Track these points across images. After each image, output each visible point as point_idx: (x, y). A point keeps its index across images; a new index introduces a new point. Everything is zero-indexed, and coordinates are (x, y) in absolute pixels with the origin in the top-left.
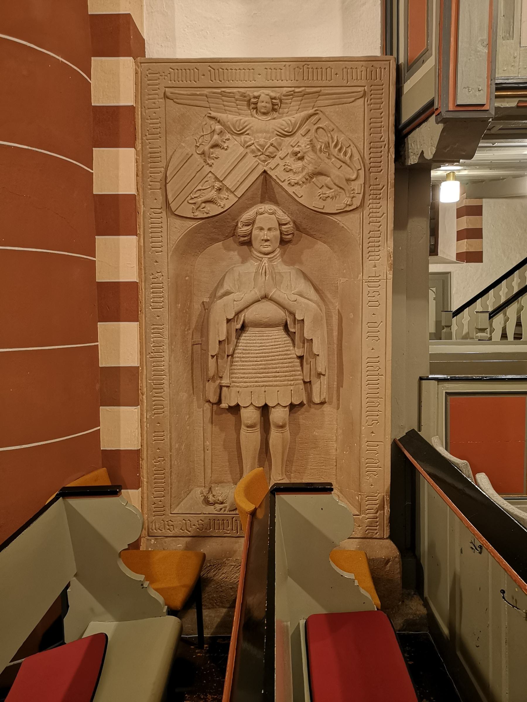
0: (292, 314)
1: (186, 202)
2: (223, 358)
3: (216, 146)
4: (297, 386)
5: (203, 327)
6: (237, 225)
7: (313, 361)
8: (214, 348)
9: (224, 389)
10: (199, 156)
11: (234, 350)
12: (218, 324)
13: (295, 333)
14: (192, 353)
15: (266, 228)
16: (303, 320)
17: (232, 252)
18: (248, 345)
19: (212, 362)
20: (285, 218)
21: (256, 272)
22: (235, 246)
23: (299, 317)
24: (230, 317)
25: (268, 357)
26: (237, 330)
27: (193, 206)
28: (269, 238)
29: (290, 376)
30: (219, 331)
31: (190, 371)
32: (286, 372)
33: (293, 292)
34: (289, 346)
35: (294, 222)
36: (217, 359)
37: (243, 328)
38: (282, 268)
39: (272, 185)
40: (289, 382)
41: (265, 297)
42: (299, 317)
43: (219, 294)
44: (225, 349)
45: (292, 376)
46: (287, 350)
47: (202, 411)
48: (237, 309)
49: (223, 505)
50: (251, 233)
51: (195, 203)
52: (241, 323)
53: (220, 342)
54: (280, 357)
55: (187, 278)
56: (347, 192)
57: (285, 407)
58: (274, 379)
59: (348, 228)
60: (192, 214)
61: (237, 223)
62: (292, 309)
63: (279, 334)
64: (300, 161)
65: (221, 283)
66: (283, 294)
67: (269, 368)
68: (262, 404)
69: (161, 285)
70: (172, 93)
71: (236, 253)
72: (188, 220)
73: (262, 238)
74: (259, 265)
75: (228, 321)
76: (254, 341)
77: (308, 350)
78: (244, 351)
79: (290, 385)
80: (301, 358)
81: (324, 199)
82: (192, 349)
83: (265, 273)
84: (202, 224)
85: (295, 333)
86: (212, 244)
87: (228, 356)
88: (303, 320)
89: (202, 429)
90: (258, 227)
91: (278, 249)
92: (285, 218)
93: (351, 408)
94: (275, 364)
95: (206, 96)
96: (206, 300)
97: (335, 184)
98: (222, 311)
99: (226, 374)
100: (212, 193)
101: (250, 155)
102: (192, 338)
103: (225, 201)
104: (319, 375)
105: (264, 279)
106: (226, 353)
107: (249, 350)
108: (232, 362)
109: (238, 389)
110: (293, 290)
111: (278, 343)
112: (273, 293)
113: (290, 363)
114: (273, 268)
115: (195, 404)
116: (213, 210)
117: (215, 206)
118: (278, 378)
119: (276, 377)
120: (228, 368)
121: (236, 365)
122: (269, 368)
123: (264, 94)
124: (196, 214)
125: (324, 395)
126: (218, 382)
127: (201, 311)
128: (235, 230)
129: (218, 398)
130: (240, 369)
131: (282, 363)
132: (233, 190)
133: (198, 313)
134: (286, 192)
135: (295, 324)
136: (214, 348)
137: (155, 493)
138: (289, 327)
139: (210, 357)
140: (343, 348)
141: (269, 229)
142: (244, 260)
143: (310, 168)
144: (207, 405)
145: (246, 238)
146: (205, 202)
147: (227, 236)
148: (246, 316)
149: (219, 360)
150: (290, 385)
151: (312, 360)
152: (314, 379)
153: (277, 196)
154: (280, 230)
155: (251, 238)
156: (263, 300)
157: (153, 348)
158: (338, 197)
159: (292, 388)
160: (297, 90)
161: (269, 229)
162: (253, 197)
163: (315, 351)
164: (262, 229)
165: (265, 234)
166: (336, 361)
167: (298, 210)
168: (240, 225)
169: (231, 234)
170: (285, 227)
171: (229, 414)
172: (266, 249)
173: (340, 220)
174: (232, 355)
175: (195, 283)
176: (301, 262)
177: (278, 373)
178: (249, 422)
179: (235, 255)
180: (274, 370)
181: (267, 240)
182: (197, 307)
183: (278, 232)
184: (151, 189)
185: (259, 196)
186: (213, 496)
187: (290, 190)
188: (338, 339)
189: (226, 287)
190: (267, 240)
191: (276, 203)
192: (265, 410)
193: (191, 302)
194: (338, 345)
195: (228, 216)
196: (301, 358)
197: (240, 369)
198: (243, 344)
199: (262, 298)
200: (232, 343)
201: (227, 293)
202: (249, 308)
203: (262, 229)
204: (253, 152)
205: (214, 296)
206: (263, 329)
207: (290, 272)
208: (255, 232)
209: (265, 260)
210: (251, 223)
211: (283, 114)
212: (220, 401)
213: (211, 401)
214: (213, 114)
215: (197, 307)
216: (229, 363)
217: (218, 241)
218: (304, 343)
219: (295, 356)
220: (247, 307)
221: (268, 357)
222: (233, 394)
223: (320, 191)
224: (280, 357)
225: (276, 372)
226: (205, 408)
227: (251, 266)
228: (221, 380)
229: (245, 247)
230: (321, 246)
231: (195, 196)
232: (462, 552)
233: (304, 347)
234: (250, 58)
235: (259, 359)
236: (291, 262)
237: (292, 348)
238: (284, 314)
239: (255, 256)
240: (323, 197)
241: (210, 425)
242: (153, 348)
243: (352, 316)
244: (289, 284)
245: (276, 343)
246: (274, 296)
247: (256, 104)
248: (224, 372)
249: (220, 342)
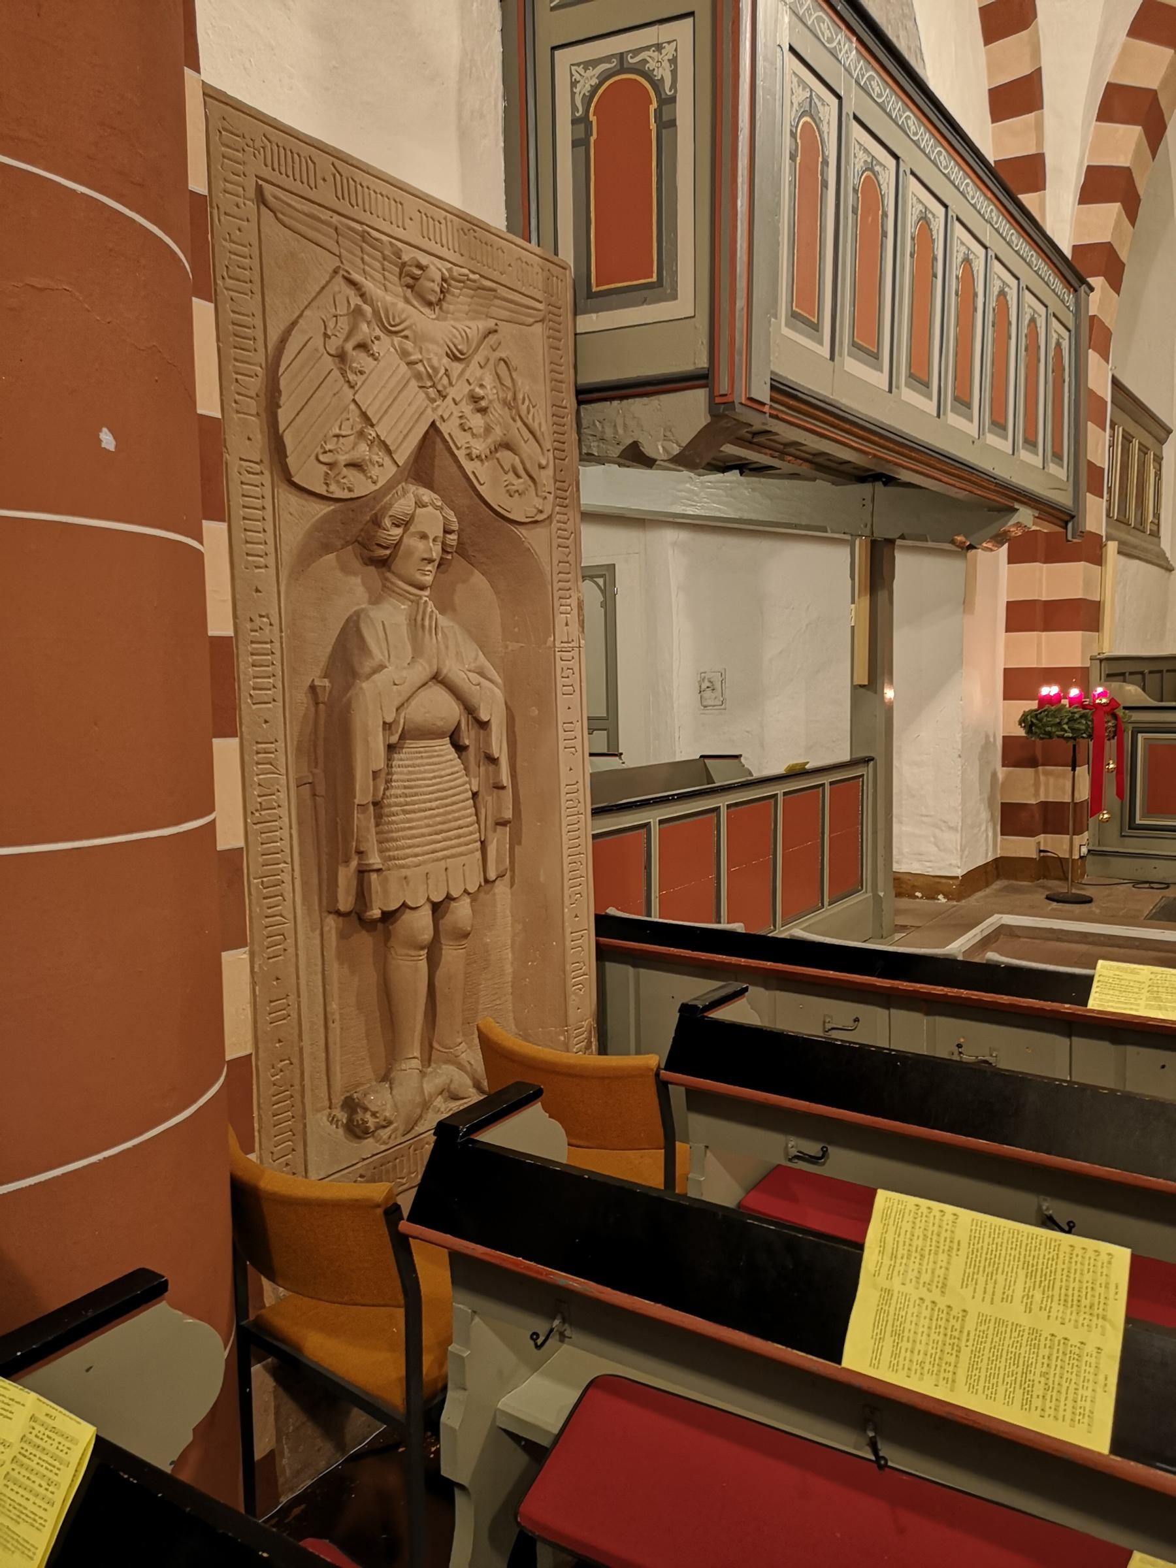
0: (470, 710)
3: (362, 346)
10: (330, 358)
22: (356, 564)
25: (446, 797)
39: (434, 450)
47: (318, 938)
49: (392, 1127)
60: (325, 487)
62: (475, 701)
64: (479, 415)
67: (450, 821)
69: (268, 646)
70: (275, 197)
71: (359, 580)
72: (314, 499)
78: (406, 791)
90: (419, 533)
93: (542, 879)
95: (336, 229)
97: (525, 469)
101: (414, 383)
109: (404, 872)
117: (361, 476)
123: (437, 269)
134: (460, 467)
137: (275, 1150)
143: (498, 434)
153: (436, 474)
157: (259, 800)
160: (472, 276)
164: (424, 536)
171: (364, 932)
184: (238, 412)
186: (374, 1115)
187: (468, 466)
191: (430, 486)
204: (418, 376)
210: (405, 523)
211: (448, 312)
214: (356, 276)
221: (446, 797)
232: (88, 1370)
234: (428, 195)
235: (434, 804)
242: (259, 800)
243: (535, 712)
247: (416, 278)
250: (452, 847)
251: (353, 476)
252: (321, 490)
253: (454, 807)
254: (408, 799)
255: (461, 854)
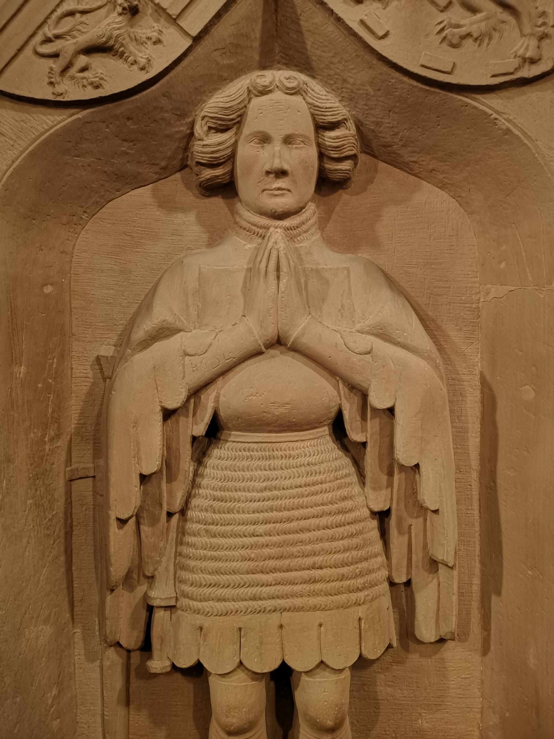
1: (28, 51)
2: (154, 521)
4: (375, 604)
5: (96, 433)
6: (192, 134)
7: (416, 524)
8: (125, 496)
9: (159, 615)
11: (187, 502)
12: (136, 424)
13: (364, 444)
14: (69, 503)
15: (278, 136)
16: (391, 411)
17: (180, 215)
18: (230, 484)
19: (120, 542)
20: (333, 106)
21: (249, 270)
22: (189, 197)
23: (378, 400)
24: (172, 404)
25: (289, 520)
26: (194, 439)
27: (50, 63)
28: (286, 167)
29: (356, 576)
30: (139, 444)
31: (63, 558)
32: (344, 564)
33: (358, 326)
34: (350, 484)
35: (359, 126)
36: (138, 523)
37: (215, 430)
38: (323, 257)
40: (353, 596)
41: (278, 342)
42: (378, 400)
43: (139, 334)
44: (160, 494)
45: (361, 574)
46: (344, 499)
47: (98, 670)
48: (194, 378)
50: (232, 157)
51: (55, 56)
52: (207, 418)
53: (143, 478)
54: (324, 521)
55: (48, 289)
56: (525, 19)
57: (341, 671)
58: (307, 587)
59: (525, 134)
60: (50, 89)
61: (192, 125)
62: (358, 379)
63: (319, 447)
65: (146, 306)
66: (323, 331)
67: (292, 556)
68: (272, 665)
71: (192, 217)
73: (267, 167)
74: (257, 249)
75: (168, 414)
76: (247, 474)
77: (403, 491)
79: (358, 604)
80: (382, 517)
81: (455, 41)
82: (69, 493)
83: (278, 269)
84: (85, 122)
85: (364, 444)
86: (120, 192)
87: (170, 515)
88: (391, 411)
89: (99, 720)
91: (311, 207)
92: (333, 106)
94: (310, 542)
96: (106, 350)
98: (149, 384)
99: (164, 569)
100: (109, 20)
102: (69, 461)
103: (150, 50)
104: (433, 565)
105: (273, 288)
106: (164, 503)
107: (231, 500)
108: (182, 532)
109: (199, 620)
110: (356, 317)
111: (319, 478)
112: (303, 329)
113: (352, 536)
114: (300, 259)
115: (79, 648)
116: (116, 76)
118: (318, 586)
119: (315, 581)
120: (170, 550)
121: (193, 545)
122: (292, 556)
124: (59, 89)
125: (451, 625)
126: (142, 589)
127: (93, 384)
128: (186, 149)
129: (142, 636)
130: (204, 558)
131: (333, 539)
132: (174, 11)
133: (85, 389)
135: (364, 417)
136: (125, 496)
138: (347, 426)
139: (113, 524)
140: (499, 481)
141: (288, 140)
142: (215, 237)
144: (111, 653)
145: (219, 172)
146: (91, 50)
147: (164, 168)
148: (222, 399)
149: (145, 528)
150: (358, 604)
151: (413, 521)
152: (420, 577)
153: (309, 44)
154: (319, 145)
155: (232, 173)
156: (272, 352)
158: (496, 35)
159: (361, 611)
161: (288, 140)
162: (238, 46)
163: (430, 504)
164: (265, 139)
165: (275, 155)
166: (477, 517)
167: (371, 83)
168: (199, 129)
169: (177, 163)
170: (333, 134)
172: (278, 200)
173: (499, 108)
174: (183, 512)
175: (74, 303)
176: (375, 243)
177: (321, 568)
178: (234, 721)
179: (188, 224)
180: (309, 561)
181: (281, 173)
182: (81, 373)
183: (313, 152)
185: (256, 44)
188: (481, 455)
189: (161, 313)
190: (281, 173)
191: (306, 66)
192: (282, 681)
193: (62, 357)
194: (481, 474)
195: (164, 101)
196: (382, 517)
197: (204, 558)
198: (213, 483)
199: (270, 346)
200: (181, 477)
201: (164, 332)
202: (230, 375)
203: (265, 139)
205: (125, 343)
206: (274, 437)
207: (348, 269)
208: (246, 151)
209: (277, 232)
212: (146, 647)
213: (123, 643)
215: (81, 373)
216: (173, 535)
217: (138, 182)
218: (390, 474)
219: (367, 513)
220: (224, 373)
221: (289, 520)
222: (185, 634)
223: (442, 17)
224: (324, 521)
225: (313, 567)
226: (107, 663)
227: (235, 254)
228: (150, 587)
229: (217, 202)
230: (430, 197)
231: (57, 31)
233: (390, 485)
235: (261, 529)
236: (348, 241)
237: (357, 489)
238: (332, 392)
239: (244, 224)
240: (453, 35)
241: (121, 711)
244: (470, 276)
245: (310, 479)
246: (304, 340)
248: (159, 562)
249: (143, 478)
250: (294, 595)
251: (101, 65)
252: (47, 94)
253: (302, 536)
254: (217, 516)
255: (315, 608)
